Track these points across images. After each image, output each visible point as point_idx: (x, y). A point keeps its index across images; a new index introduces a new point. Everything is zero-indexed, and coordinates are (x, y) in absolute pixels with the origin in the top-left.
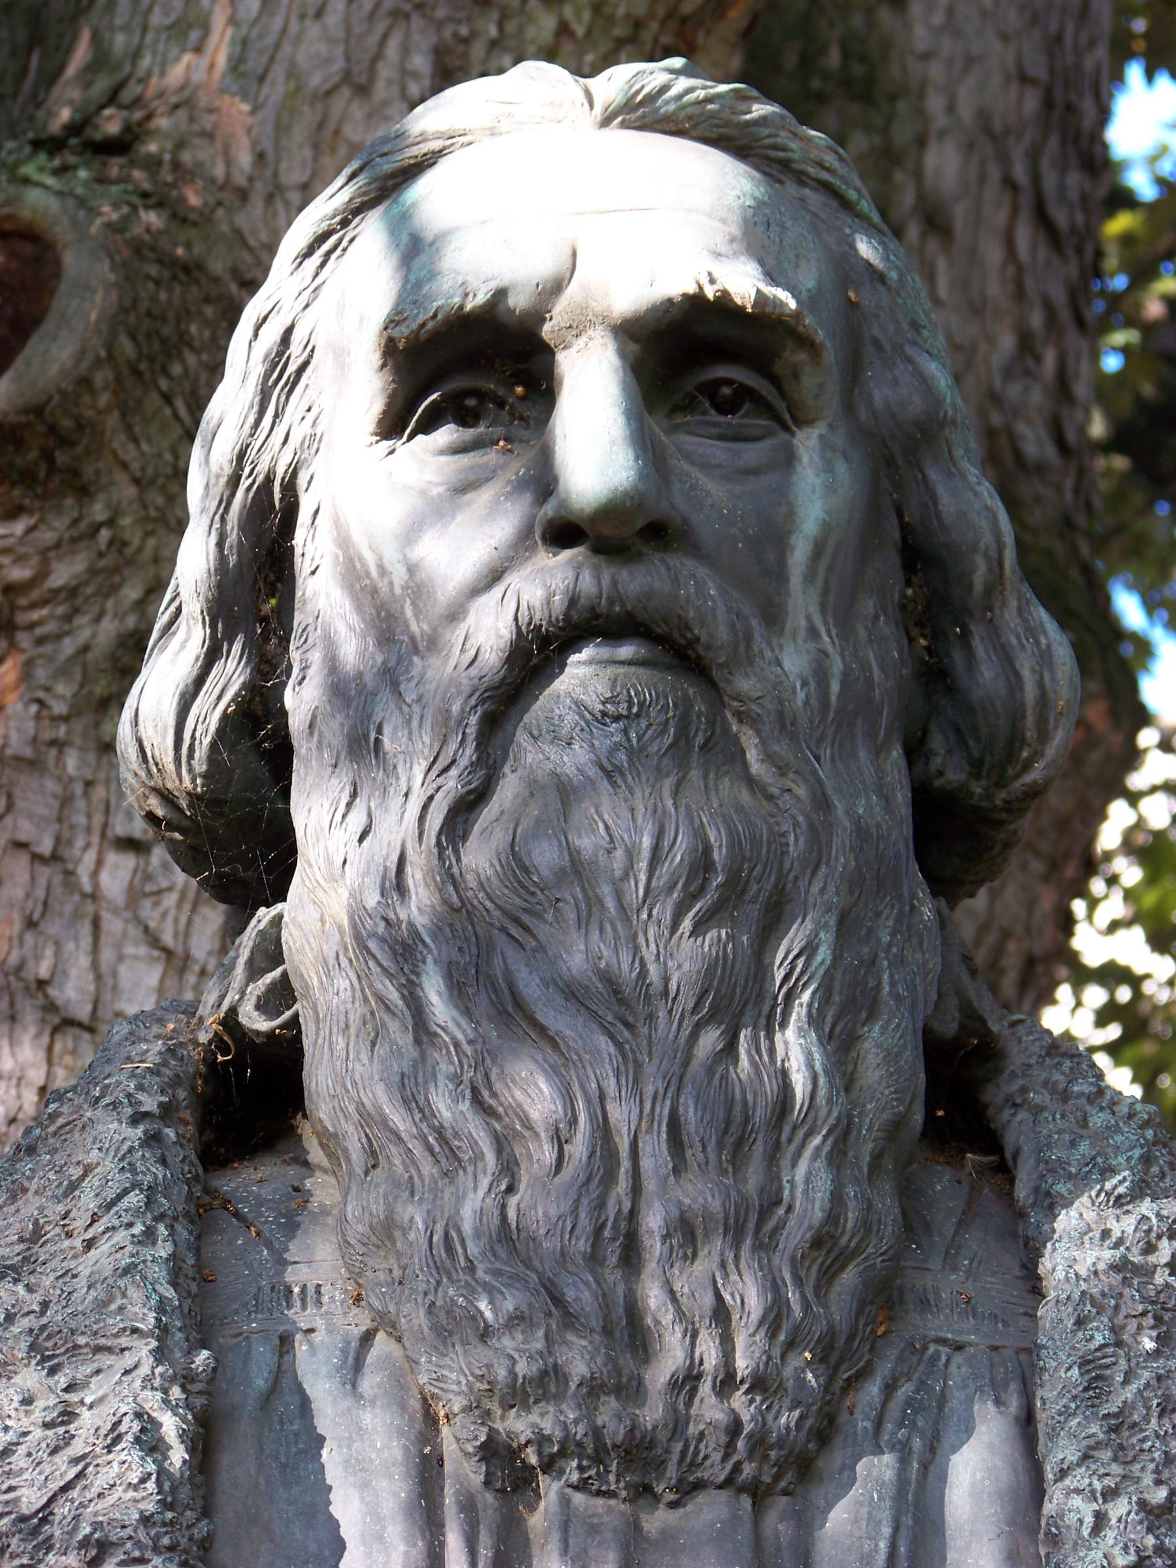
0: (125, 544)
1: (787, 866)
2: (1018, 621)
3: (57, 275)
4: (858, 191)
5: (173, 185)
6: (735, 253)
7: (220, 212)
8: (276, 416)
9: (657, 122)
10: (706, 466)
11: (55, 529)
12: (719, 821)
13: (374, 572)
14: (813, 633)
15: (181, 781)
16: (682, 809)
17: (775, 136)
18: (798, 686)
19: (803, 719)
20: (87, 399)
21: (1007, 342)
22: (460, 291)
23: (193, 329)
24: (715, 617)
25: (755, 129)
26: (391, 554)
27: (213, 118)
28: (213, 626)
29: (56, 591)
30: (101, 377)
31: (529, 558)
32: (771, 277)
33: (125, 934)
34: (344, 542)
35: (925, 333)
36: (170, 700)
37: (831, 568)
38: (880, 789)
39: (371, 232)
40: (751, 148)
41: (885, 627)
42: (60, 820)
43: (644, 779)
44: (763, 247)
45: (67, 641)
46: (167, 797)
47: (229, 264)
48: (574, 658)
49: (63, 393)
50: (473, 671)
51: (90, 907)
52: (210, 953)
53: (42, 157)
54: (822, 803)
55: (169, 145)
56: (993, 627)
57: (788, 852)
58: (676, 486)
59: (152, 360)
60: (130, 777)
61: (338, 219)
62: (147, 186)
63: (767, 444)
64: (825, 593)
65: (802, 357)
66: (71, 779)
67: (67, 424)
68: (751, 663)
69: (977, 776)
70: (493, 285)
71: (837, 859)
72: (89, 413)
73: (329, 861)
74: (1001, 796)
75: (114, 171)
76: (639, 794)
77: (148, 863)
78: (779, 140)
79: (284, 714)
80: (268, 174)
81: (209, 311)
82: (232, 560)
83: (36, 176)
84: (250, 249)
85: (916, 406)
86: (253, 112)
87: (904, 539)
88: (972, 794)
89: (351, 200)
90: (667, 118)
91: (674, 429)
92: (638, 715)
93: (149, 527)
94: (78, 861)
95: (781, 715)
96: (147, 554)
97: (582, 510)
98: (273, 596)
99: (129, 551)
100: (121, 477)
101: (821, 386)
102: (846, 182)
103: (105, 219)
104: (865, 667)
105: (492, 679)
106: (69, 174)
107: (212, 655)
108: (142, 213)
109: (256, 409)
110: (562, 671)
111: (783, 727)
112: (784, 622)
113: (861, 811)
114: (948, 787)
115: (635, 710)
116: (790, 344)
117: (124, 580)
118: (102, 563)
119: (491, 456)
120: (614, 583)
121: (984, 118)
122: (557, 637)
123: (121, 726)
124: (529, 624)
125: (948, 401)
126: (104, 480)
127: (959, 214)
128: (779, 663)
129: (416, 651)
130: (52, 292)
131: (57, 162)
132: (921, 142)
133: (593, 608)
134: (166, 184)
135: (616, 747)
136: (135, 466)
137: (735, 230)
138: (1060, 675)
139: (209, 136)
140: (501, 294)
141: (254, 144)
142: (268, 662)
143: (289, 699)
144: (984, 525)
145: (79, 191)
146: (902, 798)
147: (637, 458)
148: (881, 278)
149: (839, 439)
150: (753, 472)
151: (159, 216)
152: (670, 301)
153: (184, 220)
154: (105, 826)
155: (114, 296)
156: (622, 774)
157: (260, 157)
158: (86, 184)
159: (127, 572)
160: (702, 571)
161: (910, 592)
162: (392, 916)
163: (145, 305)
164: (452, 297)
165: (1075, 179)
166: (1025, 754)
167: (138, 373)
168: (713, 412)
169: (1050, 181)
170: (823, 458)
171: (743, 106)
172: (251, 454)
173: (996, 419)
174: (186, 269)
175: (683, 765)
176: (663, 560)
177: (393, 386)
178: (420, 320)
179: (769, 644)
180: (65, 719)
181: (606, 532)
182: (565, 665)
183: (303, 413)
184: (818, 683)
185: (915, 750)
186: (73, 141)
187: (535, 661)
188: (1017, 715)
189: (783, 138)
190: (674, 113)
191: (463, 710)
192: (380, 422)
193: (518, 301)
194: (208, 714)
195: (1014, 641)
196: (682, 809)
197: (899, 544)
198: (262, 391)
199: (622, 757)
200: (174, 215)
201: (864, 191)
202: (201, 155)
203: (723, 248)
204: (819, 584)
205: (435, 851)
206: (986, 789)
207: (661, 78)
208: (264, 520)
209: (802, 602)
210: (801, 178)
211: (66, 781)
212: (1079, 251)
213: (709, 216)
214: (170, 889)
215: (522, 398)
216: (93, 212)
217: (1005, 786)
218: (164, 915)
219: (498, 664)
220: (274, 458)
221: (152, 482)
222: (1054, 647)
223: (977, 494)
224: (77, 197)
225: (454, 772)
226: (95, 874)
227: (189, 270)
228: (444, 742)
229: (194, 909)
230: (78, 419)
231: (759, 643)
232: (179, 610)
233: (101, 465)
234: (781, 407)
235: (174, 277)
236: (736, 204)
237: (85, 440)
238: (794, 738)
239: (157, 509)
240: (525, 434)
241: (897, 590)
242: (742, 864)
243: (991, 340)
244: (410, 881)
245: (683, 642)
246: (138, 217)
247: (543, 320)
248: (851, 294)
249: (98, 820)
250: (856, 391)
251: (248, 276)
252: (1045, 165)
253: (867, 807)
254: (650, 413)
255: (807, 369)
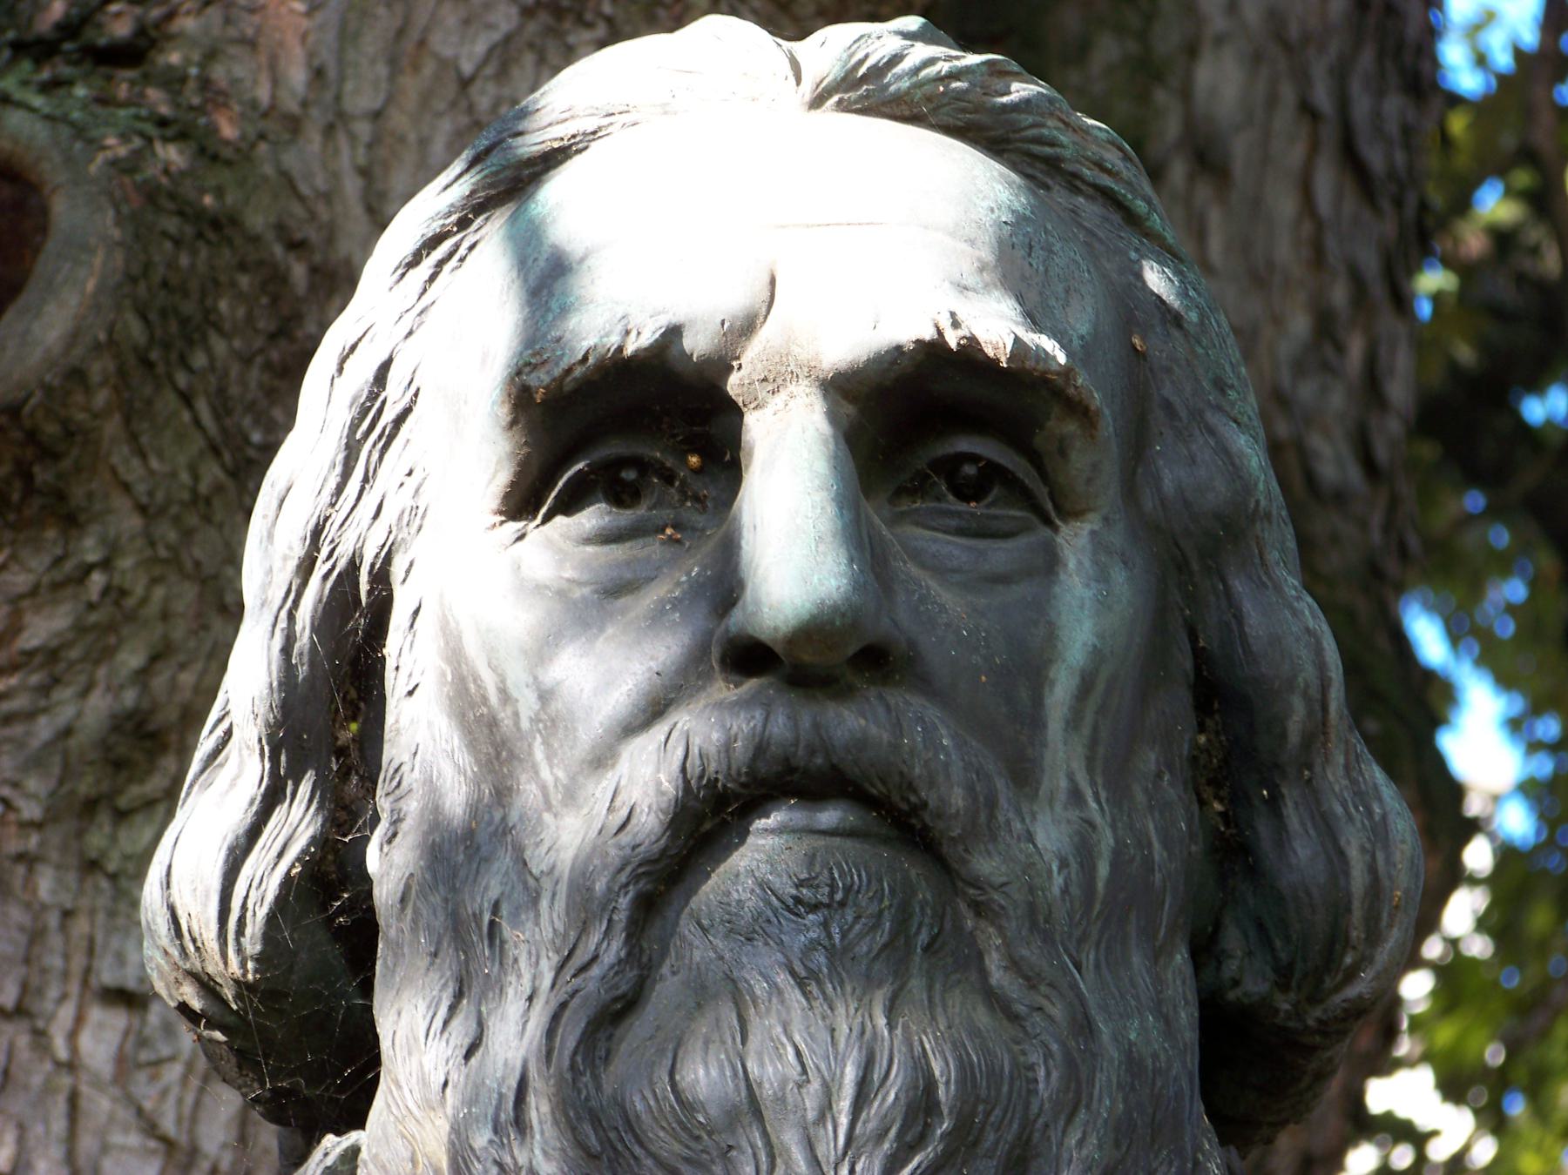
0: (124, 593)
1: (1035, 1108)
2: (1345, 782)
3: (44, 229)
4: (1149, 202)
5: (200, 110)
6: (986, 286)
7: (263, 147)
8: (366, 480)
9: (884, 104)
10: (941, 571)
11: (30, 571)
12: (947, 1048)
13: (494, 698)
14: (1076, 796)
15: (226, 964)
16: (899, 1031)
17: (1043, 125)
18: (1055, 868)
19: (1060, 914)
20: (79, 398)
21: (1300, 324)
22: (619, 328)
23: (223, 305)
24: (948, 776)
25: (1014, 115)
26: (517, 675)
27: (256, 19)
28: (275, 759)
29: (30, 654)
30: (98, 368)
31: (703, 688)
32: (1034, 319)
33: (111, 1119)
34: (455, 655)
35: (1233, 395)
36: (213, 853)
37: (1102, 710)
38: (1158, 1007)
39: (492, 235)
40: (1007, 141)
41: (1171, 790)
42: (27, 961)
43: (848, 989)
44: (1023, 278)
45: (43, 720)
46: (206, 985)
47: (272, 219)
48: (760, 824)
49: (48, 389)
50: (625, 838)
51: (66, 1081)
52: (224, 1146)
53: (26, 65)
54: (1084, 1027)
55: (196, 56)
56: (1313, 793)
57: (1036, 1092)
58: (901, 597)
59: (167, 346)
60: (159, 958)
61: (454, 218)
62: (164, 110)
63: (1022, 541)
64: (1093, 743)
65: (1071, 427)
66: (44, 907)
67: (51, 429)
68: (994, 838)
69: (1283, 985)
70: (663, 321)
71: (1100, 1100)
72: (80, 416)
73: (424, 1082)
74: (1314, 1015)
75: (123, 91)
76: (841, 1010)
77: (144, 1022)
78: (1045, 131)
79: (367, 880)
80: (328, 96)
81: (244, 281)
82: (302, 672)
83: (18, 95)
84: (301, 199)
85: (1219, 491)
86: (309, 14)
87: (1197, 668)
88: (1277, 1011)
89: (473, 192)
90: (898, 99)
91: (895, 520)
92: (842, 904)
93: (157, 571)
94: (51, 1017)
95: (1032, 909)
96: (153, 608)
97: (776, 629)
98: (354, 719)
99: (130, 602)
100: (121, 502)
101: (1095, 467)
102: (1133, 190)
103: (109, 154)
104: (1143, 843)
105: (649, 847)
106: (62, 92)
107: (272, 797)
108: (158, 147)
109: (339, 469)
110: (742, 841)
111: (1034, 926)
112: (1039, 783)
113: (1133, 1036)
114: (1246, 1001)
115: (839, 896)
116: (1056, 410)
117: (120, 641)
118: (93, 618)
119: (651, 549)
120: (816, 726)
121: (1276, 21)
122: (737, 796)
123: (147, 888)
124: (701, 777)
125: (1261, 486)
126: (98, 507)
127: (1240, 150)
128: (1030, 838)
129: (548, 806)
130: (37, 250)
131: (45, 75)
132: (1192, 51)
133: (787, 759)
134: (191, 108)
135: (813, 946)
136: (141, 489)
137: (987, 255)
138: (1397, 856)
139: (251, 44)
140: (673, 333)
141: (311, 55)
142: (345, 808)
143: (373, 860)
144: (1305, 655)
145: (76, 115)
146: (1187, 1018)
147: (851, 560)
148: (1176, 319)
149: (1117, 538)
150: (1001, 579)
151: (181, 152)
152: (899, 348)
153: (215, 158)
154: (88, 971)
155: (119, 257)
156: (819, 983)
157: (318, 74)
158: (84, 106)
159: (125, 631)
160: (933, 713)
161: (1202, 739)
162: (508, 1160)
163: (159, 273)
164: (607, 335)
165: (1395, 105)
166: (1348, 960)
167: (148, 365)
168: (951, 497)
169: (1361, 106)
170: (1096, 562)
171: (998, 84)
172: (330, 531)
173: (1283, 429)
174: (216, 224)
175: (900, 972)
176: (881, 697)
177: (526, 450)
178: (564, 364)
179: (1019, 812)
180: (37, 826)
181: (806, 658)
182: (748, 832)
183: (402, 478)
184: (1081, 865)
185: (1204, 950)
186: (68, 46)
187: (707, 826)
188: (1340, 908)
189: (1052, 128)
190: (908, 92)
191: (609, 889)
192: (507, 497)
193: (697, 343)
194: (265, 876)
195: (1339, 810)
196: (899, 1031)
197: (1192, 677)
198: (348, 446)
199: (820, 958)
200: (202, 150)
201: (1156, 201)
202: (239, 71)
203: (971, 280)
204: (1086, 731)
205: (568, 1076)
206: (1295, 1005)
207: (894, 44)
208: (347, 618)
209: (1062, 757)
210: (1073, 182)
211: (37, 910)
212: (1399, 203)
213: (953, 234)
214: (172, 1059)
215: (697, 472)
216: (95, 145)
217: (1321, 1001)
218: (164, 1093)
219: (658, 830)
220: (360, 536)
221: (162, 511)
222: (1391, 817)
223: (1295, 613)
224: (72, 124)
225: (596, 971)
226: (73, 1036)
227: (220, 226)
228: (584, 929)
229: (201, 1091)
230: (65, 423)
231: (1005, 811)
232: (229, 733)
233: (94, 486)
234: (1042, 492)
235: (200, 235)
236: (988, 219)
237: (75, 452)
238: (1048, 938)
239: (169, 547)
240: (699, 520)
241: (1189, 738)
242: (975, 1106)
243: (1277, 321)
244: (533, 1115)
245: (904, 807)
246: (154, 154)
247: (729, 369)
248: (1137, 341)
249: (78, 962)
250: (1140, 470)
251: (298, 236)
252: (1356, 88)
253: (1142, 1031)
254: (867, 495)
255: (1078, 444)
